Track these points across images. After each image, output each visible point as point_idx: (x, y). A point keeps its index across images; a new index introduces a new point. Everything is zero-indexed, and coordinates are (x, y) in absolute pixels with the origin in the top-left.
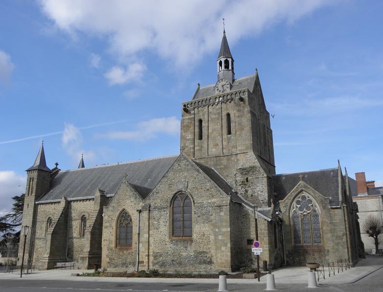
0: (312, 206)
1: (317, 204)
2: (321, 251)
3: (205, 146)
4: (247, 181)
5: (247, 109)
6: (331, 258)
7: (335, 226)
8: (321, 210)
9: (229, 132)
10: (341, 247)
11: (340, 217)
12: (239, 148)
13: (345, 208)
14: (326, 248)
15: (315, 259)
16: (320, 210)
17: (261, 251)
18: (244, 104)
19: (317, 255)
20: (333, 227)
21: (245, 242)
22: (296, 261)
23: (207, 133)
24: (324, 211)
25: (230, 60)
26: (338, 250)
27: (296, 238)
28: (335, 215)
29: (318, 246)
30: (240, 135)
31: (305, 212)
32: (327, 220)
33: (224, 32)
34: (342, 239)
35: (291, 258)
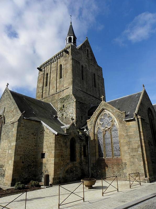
0: (112, 121)
1: (115, 119)
2: (119, 163)
3: (48, 89)
4: (63, 107)
5: (70, 57)
6: (128, 171)
7: (130, 138)
8: (119, 125)
9: (61, 77)
10: (136, 160)
11: (135, 129)
12: (65, 86)
13: (140, 120)
14: (124, 161)
15: (114, 172)
16: (118, 125)
17: (49, 165)
18: (69, 55)
19: (115, 169)
20: (128, 139)
21: (40, 156)
22: (98, 173)
23: (49, 81)
24: (121, 125)
25: (72, 37)
26: (133, 163)
27: (100, 152)
28: (130, 127)
29: (117, 160)
30: (66, 77)
31: (106, 128)
32: (123, 134)
33: (71, 23)
34: (138, 151)
35: (95, 171)
